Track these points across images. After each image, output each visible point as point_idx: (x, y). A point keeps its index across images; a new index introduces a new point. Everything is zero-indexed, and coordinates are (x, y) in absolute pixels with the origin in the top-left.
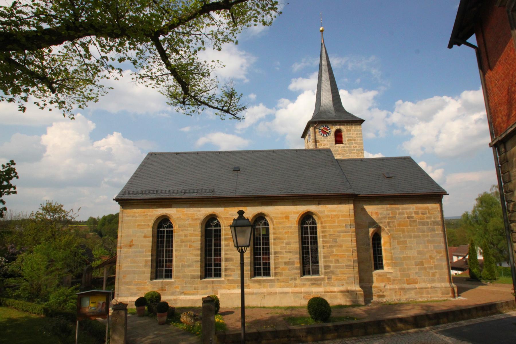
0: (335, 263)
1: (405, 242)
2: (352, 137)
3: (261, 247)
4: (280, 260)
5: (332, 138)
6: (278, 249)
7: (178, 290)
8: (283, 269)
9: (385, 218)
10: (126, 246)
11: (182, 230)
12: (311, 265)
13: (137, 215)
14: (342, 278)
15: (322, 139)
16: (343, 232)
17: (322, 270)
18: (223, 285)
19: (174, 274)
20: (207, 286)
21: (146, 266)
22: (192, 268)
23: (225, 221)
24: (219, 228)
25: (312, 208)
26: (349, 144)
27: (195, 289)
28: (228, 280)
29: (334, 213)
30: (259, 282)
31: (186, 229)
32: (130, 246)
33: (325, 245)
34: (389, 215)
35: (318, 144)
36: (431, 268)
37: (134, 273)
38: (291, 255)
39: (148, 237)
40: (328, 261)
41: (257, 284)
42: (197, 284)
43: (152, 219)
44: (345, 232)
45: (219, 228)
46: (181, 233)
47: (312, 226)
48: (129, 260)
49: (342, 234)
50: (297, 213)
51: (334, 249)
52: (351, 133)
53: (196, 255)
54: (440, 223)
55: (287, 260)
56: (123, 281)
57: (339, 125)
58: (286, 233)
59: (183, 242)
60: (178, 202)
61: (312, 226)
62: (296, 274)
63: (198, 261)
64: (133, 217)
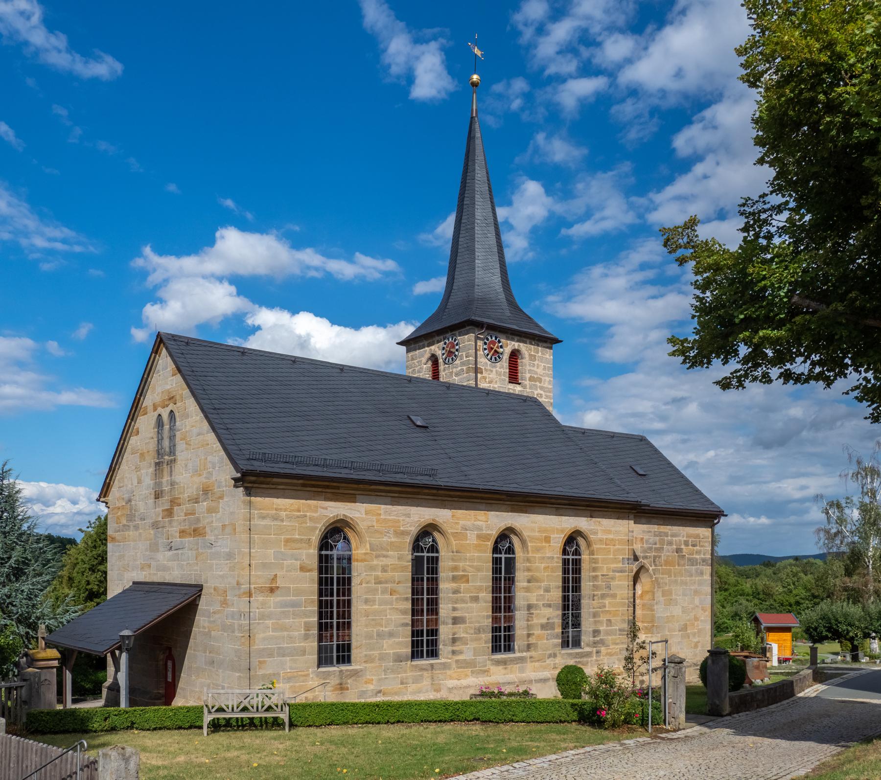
0: (607, 626)
1: (670, 593)
2: (536, 373)
3: (425, 597)
4: (535, 621)
5: (503, 366)
6: (533, 598)
7: (371, 687)
8: (539, 637)
9: (650, 549)
10: (261, 590)
11: (377, 557)
12: (570, 630)
13: (283, 514)
14: (614, 651)
15: (489, 368)
16: (618, 572)
17: (585, 638)
18: (449, 672)
19: (355, 653)
20: (422, 676)
21: (306, 637)
22: (397, 640)
23: (452, 539)
24: (435, 555)
25: (582, 523)
26: (530, 388)
27: (402, 683)
28: (457, 661)
29: (611, 536)
30: (504, 662)
31: (384, 553)
32: (272, 590)
33: (596, 593)
34: (655, 544)
35: (479, 376)
36: (694, 634)
37: (282, 653)
38: (551, 610)
39: (309, 571)
40: (599, 621)
41: (500, 667)
42: (405, 672)
43: (316, 528)
44: (621, 571)
45: (435, 555)
46: (375, 562)
47: (430, 555)
48: (269, 622)
49: (617, 574)
50: (562, 531)
51: (607, 601)
52: (536, 363)
53: (404, 612)
54: (710, 562)
55: (544, 621)
56: (260, 672)
57: (518, 341)
58: (545, 568)
59: (380, 583)
60: (537, 497)
61: (430, 555)
62: (555, 645)
63: (407, 625)
64: (275, 518)
